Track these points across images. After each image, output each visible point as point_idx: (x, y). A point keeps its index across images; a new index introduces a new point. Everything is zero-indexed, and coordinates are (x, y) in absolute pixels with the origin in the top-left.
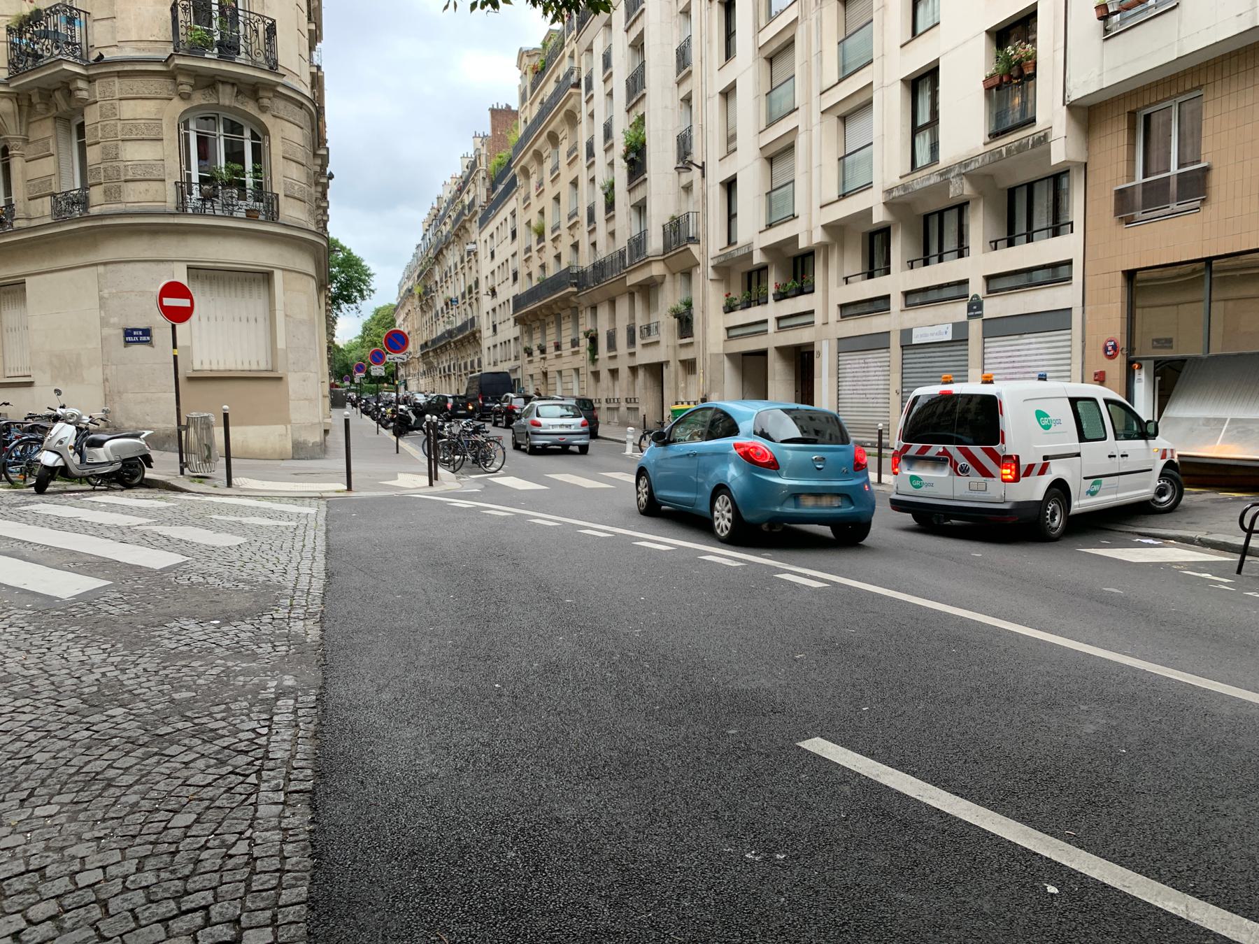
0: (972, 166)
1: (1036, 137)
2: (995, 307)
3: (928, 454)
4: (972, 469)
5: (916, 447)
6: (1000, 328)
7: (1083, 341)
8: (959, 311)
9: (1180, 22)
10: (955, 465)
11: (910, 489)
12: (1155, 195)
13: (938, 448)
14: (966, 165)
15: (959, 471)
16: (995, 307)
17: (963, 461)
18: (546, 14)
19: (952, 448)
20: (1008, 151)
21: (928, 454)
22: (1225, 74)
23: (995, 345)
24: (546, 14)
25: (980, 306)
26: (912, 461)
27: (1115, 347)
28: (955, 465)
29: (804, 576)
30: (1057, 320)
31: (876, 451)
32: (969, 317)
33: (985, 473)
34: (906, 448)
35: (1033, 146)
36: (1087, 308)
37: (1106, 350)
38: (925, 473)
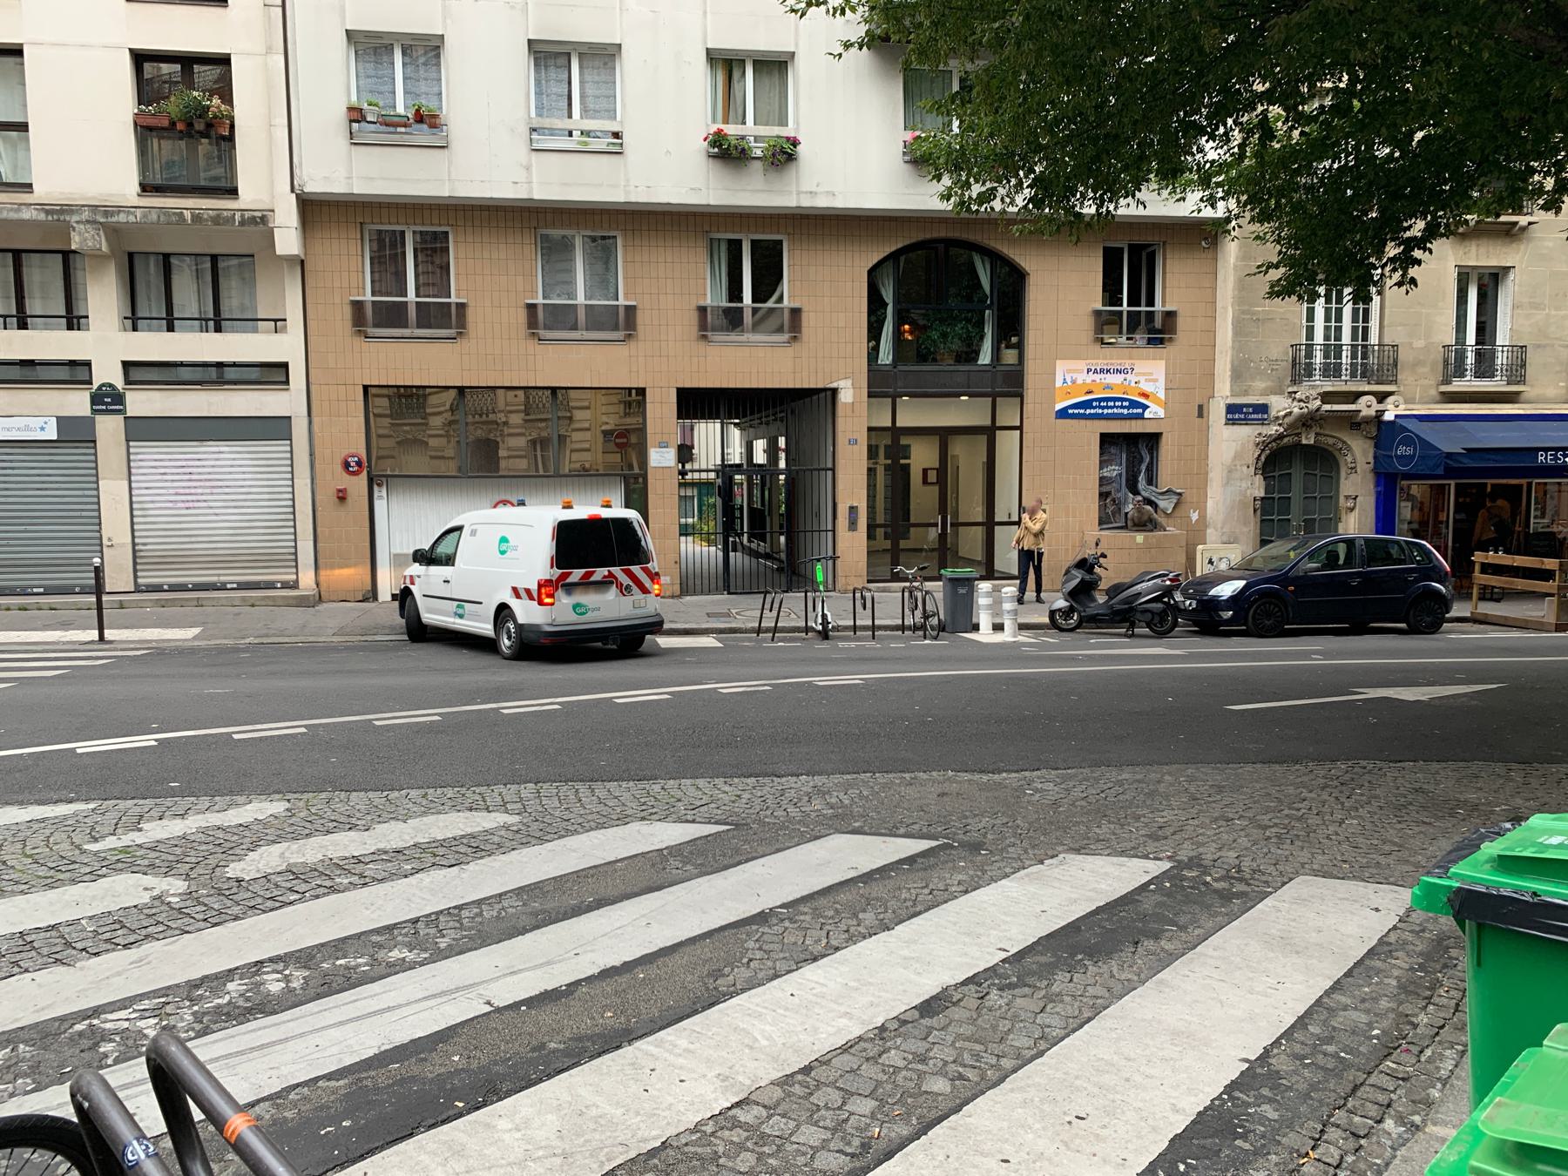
0: (122, 218)
1: (247, 215)
2: (142, 403)
3: (570, 580)
4: (635, 588)
5: (577, 574)
6: (143, 430)
7: (312, 454)
8: (77, 403)
9: (450, 163)
10: (620, 586)
11: (573, 618)
12: (392, 316)
13: (600, 573)
14: (106, 214)
15: (624, 590)
16: (142, 403)
17: (625, 580)
18: (1419, 262)
19: (616, 570)
20: (197, 218)
21: (570, 580)
22: (477, 223)
23: (150, 454)
24: (1419, 262)
25: (119, 399)
26: (570, 588)
27: (359, 463)
28: (620, 586)
29: (1091, 659)
30: (276, 428)
31: (93, 599)
32: (94, 412)
33: (645, 591)
34: (564, 576)
35: (242, 223)
36: (315, 420)
37: (346, 465)
38: (589, 599)
